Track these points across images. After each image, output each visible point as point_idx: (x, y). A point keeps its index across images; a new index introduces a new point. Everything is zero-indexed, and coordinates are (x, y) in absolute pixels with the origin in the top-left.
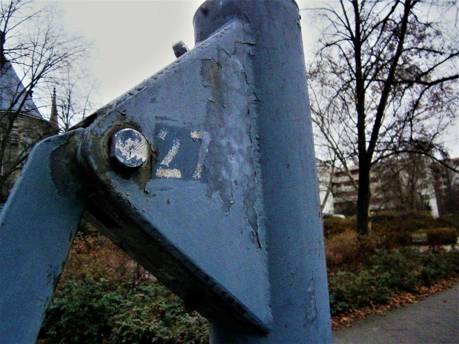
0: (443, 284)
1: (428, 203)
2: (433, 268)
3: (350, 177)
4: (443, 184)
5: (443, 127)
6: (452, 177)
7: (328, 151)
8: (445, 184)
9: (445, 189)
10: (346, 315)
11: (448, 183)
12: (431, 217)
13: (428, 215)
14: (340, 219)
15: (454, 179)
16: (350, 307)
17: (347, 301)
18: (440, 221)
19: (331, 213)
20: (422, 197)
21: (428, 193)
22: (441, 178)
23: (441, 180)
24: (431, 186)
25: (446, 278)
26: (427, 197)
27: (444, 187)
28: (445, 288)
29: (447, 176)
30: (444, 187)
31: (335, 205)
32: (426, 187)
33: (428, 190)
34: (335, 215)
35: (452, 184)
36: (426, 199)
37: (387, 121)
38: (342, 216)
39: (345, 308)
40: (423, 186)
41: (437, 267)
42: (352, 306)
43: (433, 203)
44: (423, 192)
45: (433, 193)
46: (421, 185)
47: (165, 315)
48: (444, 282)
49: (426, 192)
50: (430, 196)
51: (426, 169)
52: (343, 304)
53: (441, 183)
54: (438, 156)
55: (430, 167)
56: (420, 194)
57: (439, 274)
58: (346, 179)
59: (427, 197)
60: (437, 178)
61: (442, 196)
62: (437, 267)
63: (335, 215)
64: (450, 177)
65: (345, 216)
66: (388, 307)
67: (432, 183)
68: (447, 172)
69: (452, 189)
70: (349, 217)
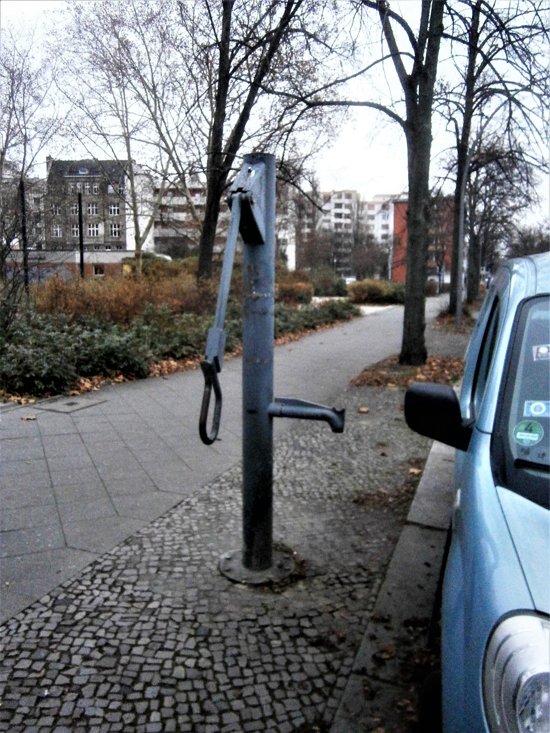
0: (290, 337)
1: (285, 251)
2: (283, 321)
3: (188, 199)
4: (306, 226)
5: (319, 147)
6: (319, 218)
7: (159, 154)
8: (309, 227)
9: (308, 234)
10: (191, 360)
11: (312, 226)
12: (286, 268)
13: (282, 266)
14: (166, 261)
15: (320, 221)
16: (195, 353)
17: (191, 345)
18: (297, 275)
19: (152, 251)
20: (278, 241)
21: (287, 237)
22: (306, 216)
23: (306, 220)
24: (292, 227)
25: (293, 332)
26: (285, 242)
27: (307, 230)
28: (291, 340)
29: (311, 216)
30: (307, 230)
31: (156, 240)
32: (285, 228)
33: (287, 231)
34: (158, 255)
35: (317, 227)
36: (283, 244)
37: (251, 126)
38: (168, 258)
39: (189, 352)
40: (282, 226)
41: (286, 320)
42: (197, 351)
43: (291, 251)
44: (281, 235)
45: (293, 238)
46: (280, 224)
47: (214, 251)
48: (292, 336)
49: (285, 235)
50: (288, 241)
51: (290, 202)
52: (189, 348)
53: (304, 224)
54: (306, 187)
55: (295, 201)
56: (277, 236)
57: (287, 328)
58: (181, 201)
59: (285, 242)
60: (300, 217)
61: (302, 243)
62: (286, 320)
63: (158, 255)
64: (316, 218)
65: (173, 257)
66: (234, 354)
67: (294, 223)
68: (314, 212)
69: (316, 234)
70: (179, 259)
